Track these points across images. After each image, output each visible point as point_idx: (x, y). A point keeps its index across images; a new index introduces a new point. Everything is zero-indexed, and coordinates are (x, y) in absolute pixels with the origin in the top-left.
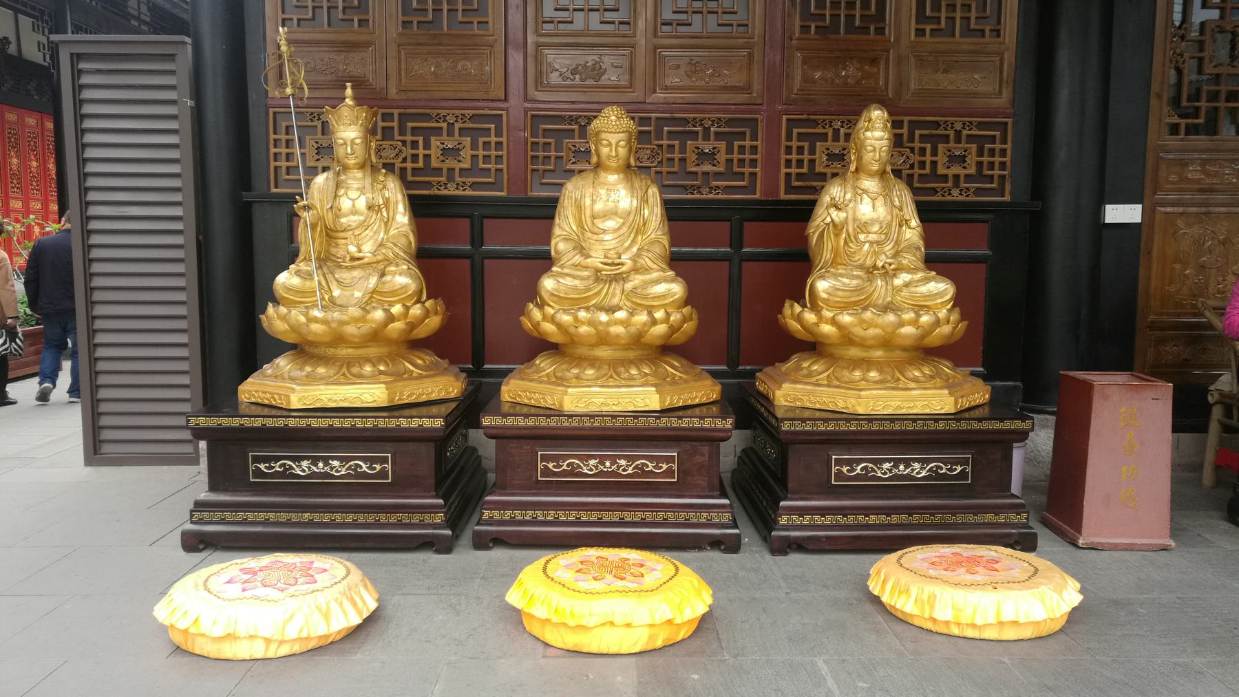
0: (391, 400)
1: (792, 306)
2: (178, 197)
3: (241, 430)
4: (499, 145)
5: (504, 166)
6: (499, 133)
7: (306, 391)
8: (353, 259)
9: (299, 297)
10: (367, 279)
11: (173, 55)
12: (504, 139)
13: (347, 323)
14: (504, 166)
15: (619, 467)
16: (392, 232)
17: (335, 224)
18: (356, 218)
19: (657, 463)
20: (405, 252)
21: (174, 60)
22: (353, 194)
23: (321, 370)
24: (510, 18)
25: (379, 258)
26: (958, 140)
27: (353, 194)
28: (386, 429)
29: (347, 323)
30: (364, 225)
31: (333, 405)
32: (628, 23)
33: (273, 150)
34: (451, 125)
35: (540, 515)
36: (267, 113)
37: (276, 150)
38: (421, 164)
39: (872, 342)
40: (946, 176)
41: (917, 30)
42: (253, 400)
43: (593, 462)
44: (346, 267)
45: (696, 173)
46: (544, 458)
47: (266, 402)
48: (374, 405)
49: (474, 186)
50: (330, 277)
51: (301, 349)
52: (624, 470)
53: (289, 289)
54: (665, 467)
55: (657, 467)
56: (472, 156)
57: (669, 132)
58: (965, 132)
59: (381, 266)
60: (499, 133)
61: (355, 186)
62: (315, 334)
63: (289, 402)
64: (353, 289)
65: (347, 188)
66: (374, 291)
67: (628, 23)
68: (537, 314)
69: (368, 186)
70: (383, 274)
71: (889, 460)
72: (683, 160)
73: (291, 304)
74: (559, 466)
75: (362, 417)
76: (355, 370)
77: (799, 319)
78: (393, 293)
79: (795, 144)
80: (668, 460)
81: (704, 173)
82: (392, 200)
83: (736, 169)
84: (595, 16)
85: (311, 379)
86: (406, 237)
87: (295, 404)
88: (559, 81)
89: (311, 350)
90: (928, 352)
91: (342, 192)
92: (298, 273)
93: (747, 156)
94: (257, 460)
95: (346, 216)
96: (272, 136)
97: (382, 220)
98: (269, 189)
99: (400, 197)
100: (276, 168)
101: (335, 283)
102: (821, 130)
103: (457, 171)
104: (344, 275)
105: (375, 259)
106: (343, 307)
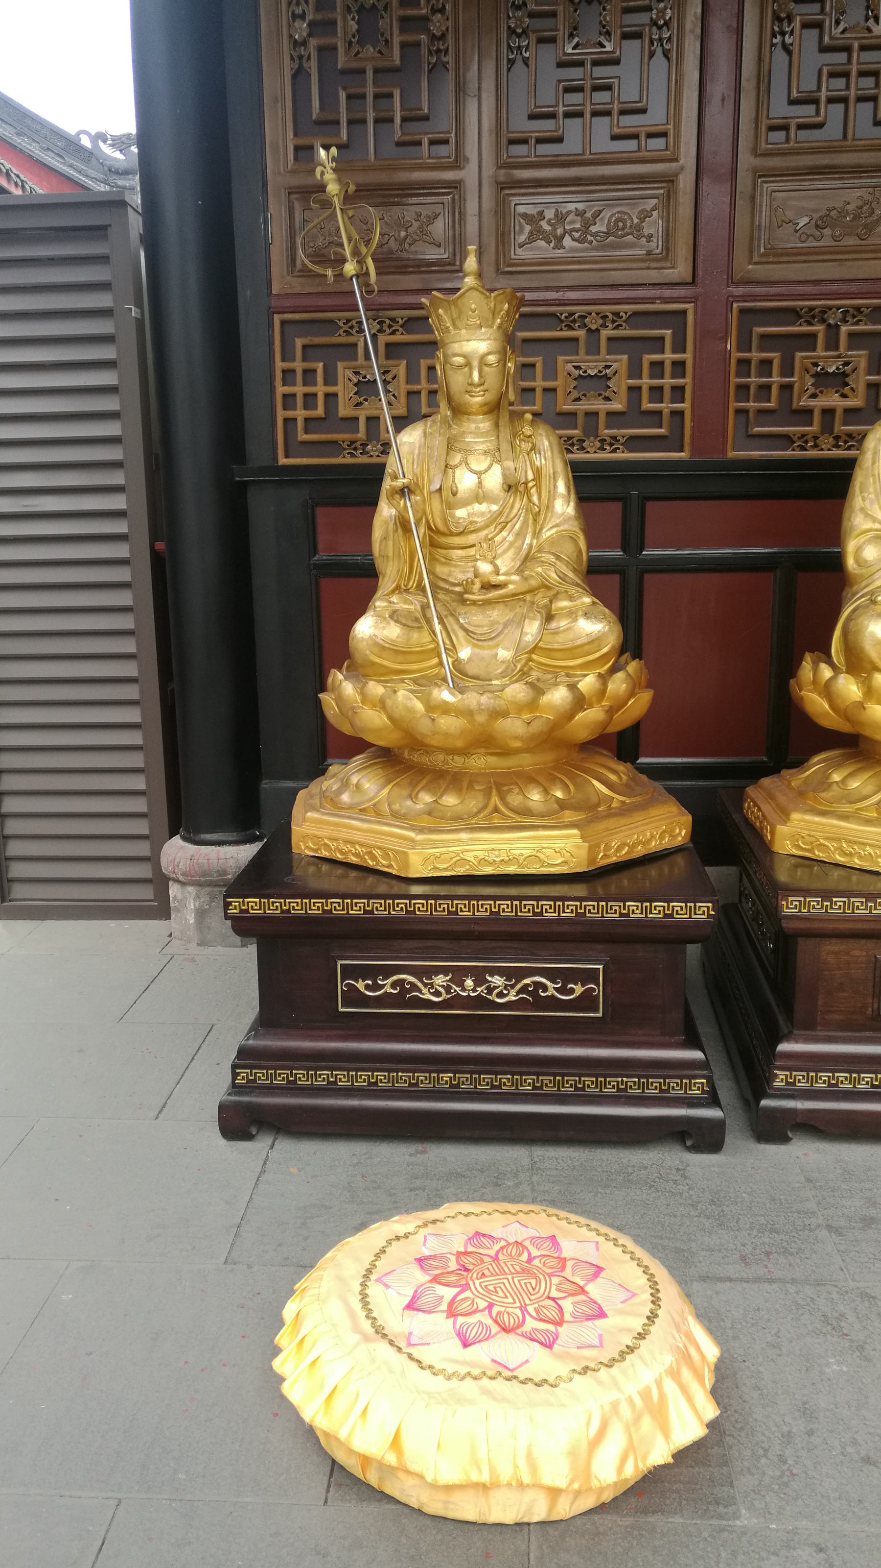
0: (592, 859)
1: (815, 669)
2: (117, 478)
3: (327, 920)
4: (679, 367)
5: (686, 406)
6: (679, 346)
7: (435, 844)
8: (488, 586)
9: (394, 662)
10: (520, 624)
11: (104, 228)
12: (688, 356)
13: (503, 714)
14: (686, 406)
15: (490, 990)
16: (547, 534)
17: (445, 521)
18: (484, 507)
19: (583, 983)
20: (575, 571)
21: (105, 237)
22: (479, 463)
23: (450, 800)
24: (708, 123)
25: (533, 583)
26: (832, 343)
27: (479, 463)
28: (602, 923)
29: (503, 714)
30: (499, 521)
31: (488, 870)
32: (664, 135)
33: (281, 389)
34: (594, 333)
35: (342, 1079)
36: (271, 325)
37: (287, 389)
38: (320, 411)
39: (517, 744)
40: (809, 412)
41: (297, 149)
42: (325, 853)
43: (440, 980)
44: (474, 603)
45: (574, 414)
46: (348, 972)
47: (354, 860)
48: (564, 870)
49: (633, 443)
50: (450, 622)
51: (403, 758)
52: (501, 995)
53: (381, 647)
54: (579, 989)
55: (563, 990)
56: (410, 393)
57: (851, 335)
58: (605, 333)
59: (541, 599)
60: (679, 346)
61: (481, 447)
62: (447, 735)
63: (406, 865)
64: (492, 645)
65: (467, 452)
66: (535, 649)
67: (664, 135)
68: (348, 689)
69: (505, 446)
70: (549, 617)
71: (444, 971)
72: (786, 388)
73: (383, 674)
74: (376, 987)
75: (469, 898)
76: (515, 799)
77: (827, 690)
78: (572, 651)
79: (298, 365)
80: (589, 976)
81: (587, 414)
82: (548, 470)
83: (647, 405)
84: (602, 125)
85: (437, 821)
86: (574, 540)
87: (418, 866)
88: (794, 243)
89: (416, 758)
90: (568, 752)
91: (457, 458)
92: (395, 616)
93: (667, 382)
94: (350, 972)
95: (465, 503)
96: (279, 365)
97: (528, 510)
98: (275, 458)
99: (560, 466)
100: (286, 420)
101: (461, 634)
102: (344, 339)
103: (602, 418)
104: (476, 619)
105: (524, 587)
106: (482, 681)
